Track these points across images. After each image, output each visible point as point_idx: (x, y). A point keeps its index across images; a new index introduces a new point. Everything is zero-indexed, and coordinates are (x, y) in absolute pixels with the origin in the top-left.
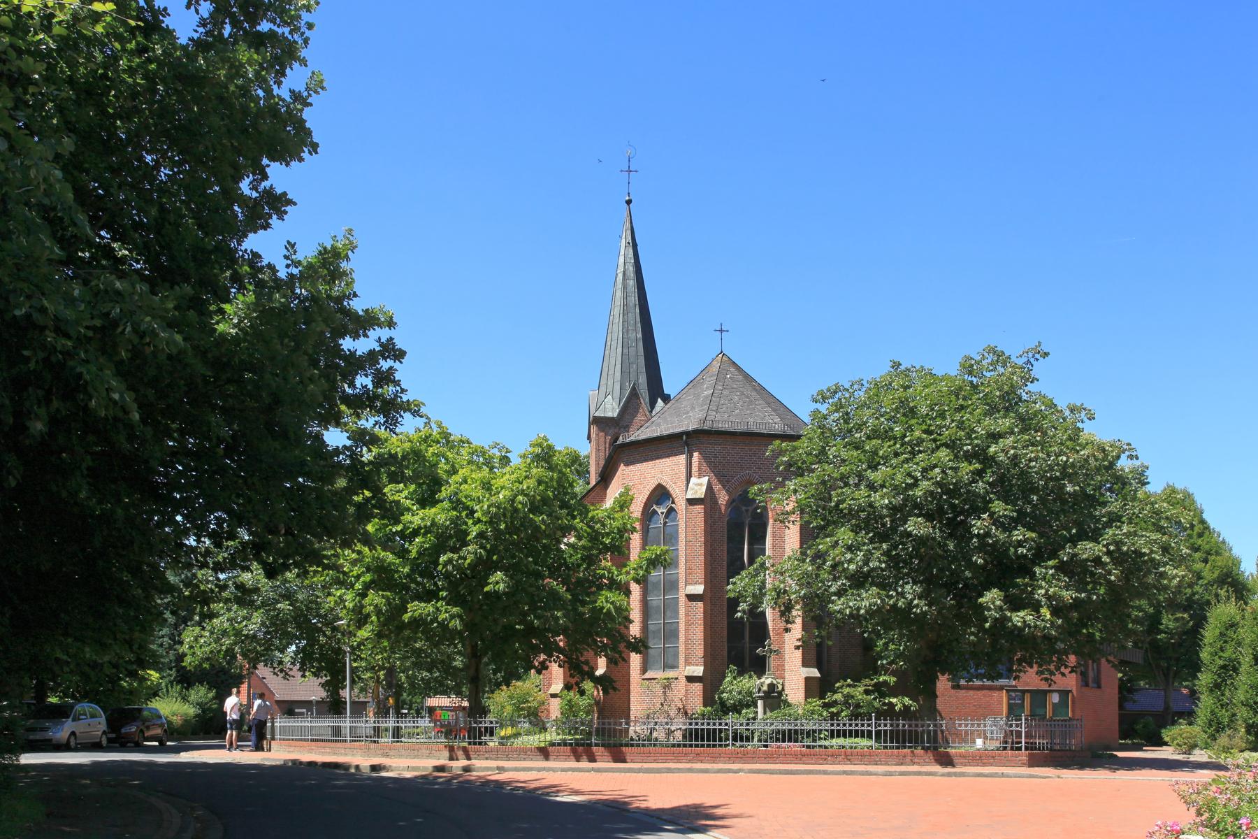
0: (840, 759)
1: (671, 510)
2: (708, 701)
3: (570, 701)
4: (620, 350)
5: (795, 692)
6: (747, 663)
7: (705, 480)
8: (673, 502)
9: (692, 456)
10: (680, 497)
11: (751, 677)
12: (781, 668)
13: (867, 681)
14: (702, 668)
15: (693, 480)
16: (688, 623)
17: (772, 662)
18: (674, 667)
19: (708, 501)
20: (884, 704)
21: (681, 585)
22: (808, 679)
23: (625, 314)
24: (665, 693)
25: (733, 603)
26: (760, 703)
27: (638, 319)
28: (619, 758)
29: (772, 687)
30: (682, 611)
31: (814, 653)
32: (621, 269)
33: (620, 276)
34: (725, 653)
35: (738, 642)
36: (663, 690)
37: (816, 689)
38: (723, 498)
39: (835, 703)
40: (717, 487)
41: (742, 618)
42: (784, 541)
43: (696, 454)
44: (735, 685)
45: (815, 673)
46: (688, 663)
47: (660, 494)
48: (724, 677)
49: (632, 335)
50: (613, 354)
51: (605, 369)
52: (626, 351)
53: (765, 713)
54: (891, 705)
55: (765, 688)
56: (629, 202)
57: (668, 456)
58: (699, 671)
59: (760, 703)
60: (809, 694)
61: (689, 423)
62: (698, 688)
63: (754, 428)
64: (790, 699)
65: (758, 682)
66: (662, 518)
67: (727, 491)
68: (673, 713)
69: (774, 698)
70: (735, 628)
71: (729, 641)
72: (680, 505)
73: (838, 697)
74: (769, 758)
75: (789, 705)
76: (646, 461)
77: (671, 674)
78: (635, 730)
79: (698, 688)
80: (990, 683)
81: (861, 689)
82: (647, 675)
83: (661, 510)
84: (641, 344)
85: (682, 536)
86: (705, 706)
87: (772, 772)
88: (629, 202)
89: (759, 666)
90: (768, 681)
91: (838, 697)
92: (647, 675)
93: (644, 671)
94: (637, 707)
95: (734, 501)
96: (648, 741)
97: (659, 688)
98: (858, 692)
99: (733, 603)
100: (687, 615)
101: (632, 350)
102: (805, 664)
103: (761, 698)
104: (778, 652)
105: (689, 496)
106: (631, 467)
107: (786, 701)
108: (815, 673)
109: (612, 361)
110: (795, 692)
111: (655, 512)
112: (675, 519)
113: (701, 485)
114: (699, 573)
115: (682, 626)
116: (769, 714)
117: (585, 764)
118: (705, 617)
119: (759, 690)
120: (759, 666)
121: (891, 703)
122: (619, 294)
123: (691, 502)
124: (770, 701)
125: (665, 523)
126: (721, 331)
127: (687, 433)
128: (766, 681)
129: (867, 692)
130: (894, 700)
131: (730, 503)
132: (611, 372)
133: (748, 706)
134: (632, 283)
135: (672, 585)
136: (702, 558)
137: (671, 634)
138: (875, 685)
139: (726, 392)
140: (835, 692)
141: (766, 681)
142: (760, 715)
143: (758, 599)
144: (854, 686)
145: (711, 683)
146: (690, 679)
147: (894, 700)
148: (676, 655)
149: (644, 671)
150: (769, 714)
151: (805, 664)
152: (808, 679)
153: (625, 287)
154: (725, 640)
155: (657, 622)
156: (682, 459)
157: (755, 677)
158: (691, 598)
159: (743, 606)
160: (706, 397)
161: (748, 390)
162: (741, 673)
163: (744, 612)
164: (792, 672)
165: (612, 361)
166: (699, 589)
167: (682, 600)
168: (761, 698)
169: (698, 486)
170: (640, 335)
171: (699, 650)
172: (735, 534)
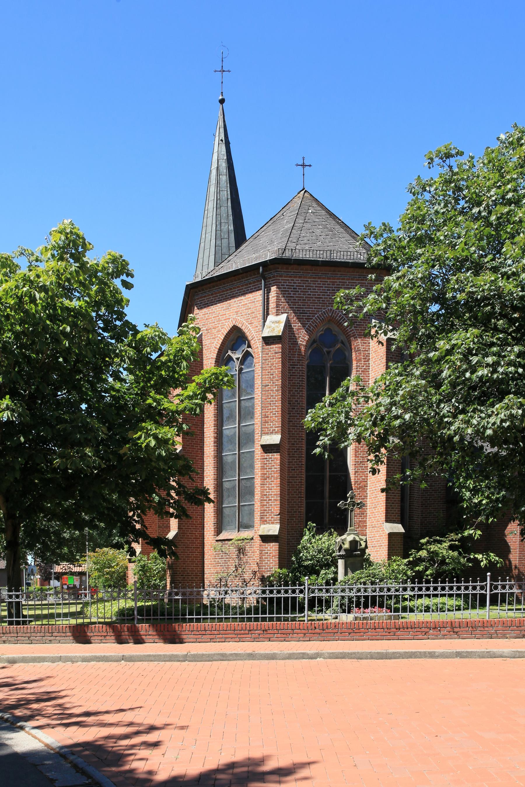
0: (444, 632)
1: (247, 355)
2: (284, 561)
3: (143, 567)
4: (213, 241)
5: (378, 552)
6: (327, 520)
7: (283, 317)
8: (249, 346)
9: (269, 291)
10: (255, 334)
11: (331, 534)
12: (363, 524)
13: (453, 536)
14: (278, 526)
15: (271, 318)
16: (264, 478)
17: (354, 517)
18: (248, 526)
19: (285, 340)
20: (469, 560)
21: (257, 437)
22: (391, 536)
23: (218, 207)
24: (238, 556)
25: (313, 436)
26: (341, 563)
27: (230, 213)
28: (174, 639)
29: (354, 543)
30: (258, 465)
31: (399, 506)
32: (215, 165)
33: (214, 172)
34: (303, 510)
35: (318, 493)
36: (237, 554)
37: (399, 546)
38: (303, 338)
39: (421, 560)
40: (296, 325)
41: (321, 455)
42: (372, 361)
43: (274, 289)
44: (315, 543)
45: (399, 528)
46: (263, 521)
47: (236, 338)
48: (302, 535)
49: (224, 228)
50: (207, 246)
51: (200, 261)
52: (219, 242)
53: (346, 574)
54: (477, 562)
55: (347, 546)
56: (222, 101)
57: (244, 294)
58: (274, 529)
59: (341, 563)
60: (391, 552)
61: (268, 255)
62: (273, 548)
63: (337, 257)
64: (372, 559)
65: (339, 539)
66: (237, 364)
67: (308, 330)
68: (247, 576)
69: (356, 557)
70: (313, 488)
71: (307, 498)
72: (257, 347)
73: (423, 553)
74: (353, 632)
75: (370, 564)
76: (220, 301)
77: (246, 534)
78: (209, 594)
79: (273, 548)
80: (40, 603)
81: (446, 545)
82: (221, 537)
83: (237, 355)
84: (232, 236)
85: (258, 383)
86: (281, 567)
87: (359, 656)
88: (222, 101)
89: (340, 524)
90: (350, 538)
91: (423, 553)
92: (221, 537)
93: (219, 530)
94: (211, 573)
95: (314, 341)
96: (221, 609)
97: (233, 551)
98: (442, 549)
99: (313, 436)
100: (263, 468)
101: (225, 242)
102: (389, 519)
103: (341, 557)
104: (361, 505)
105: (266, 334)
106: (205, 310)
107: (367, 560)
108: (399, 528)
109: (207, 253)
110: (378, 552)
111: (230, 359)
112: (251, 365)
113: (278, 322)
114: (276, 422)
115: (258, 482)
116: (350, 575)
117: (130, 649)
118: (281, 470)
119: (340, 548)
120: (340, 524)
121: (476, 559)
122: (213, 189)
123: (268, 341)
124: (351, 560)
125: (241, 370)
126: (304, 165)
127: (264, 264)
128: (349, 537)
129: (452, 548)
130: (479, 556)
131: (311, 343)
132: (206, 263)
133: (328, 566)
134: (224, 178)
135: (245, 438)
136: (279, 404)
137: (245, 491)
138: (461, 540)
139: (307, 226)
140: (419, 549)
141: (349, 537)
142: (341, 577)
143: (342, 430)
144: (440, 542)
145: (287, 543)
146: (266, 539)
147: (479, 556)
148: (251, 513)
149: (219, 530)
150: (350, 575)
151: (389, 519)
152: (391, 536)
153: (218, 182)
154: (303, 495)
155: (231, 480)
156: (258, 296)
157: (335, 534)
158: (267, 448)
159: (324, 440)
160: (287, 230)
161: (332, 223)
162: (320, 531)
163: (324, 447)
164: (375, 528)
165: (207, 253)
166: (275, 439)
167: (258, 451)
168: (341, 557)
169: (276, 324)
170: (231, 228)
171: (275, 507)
172: (317, 367)
